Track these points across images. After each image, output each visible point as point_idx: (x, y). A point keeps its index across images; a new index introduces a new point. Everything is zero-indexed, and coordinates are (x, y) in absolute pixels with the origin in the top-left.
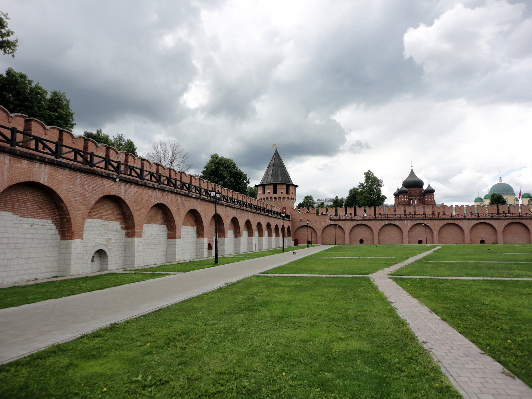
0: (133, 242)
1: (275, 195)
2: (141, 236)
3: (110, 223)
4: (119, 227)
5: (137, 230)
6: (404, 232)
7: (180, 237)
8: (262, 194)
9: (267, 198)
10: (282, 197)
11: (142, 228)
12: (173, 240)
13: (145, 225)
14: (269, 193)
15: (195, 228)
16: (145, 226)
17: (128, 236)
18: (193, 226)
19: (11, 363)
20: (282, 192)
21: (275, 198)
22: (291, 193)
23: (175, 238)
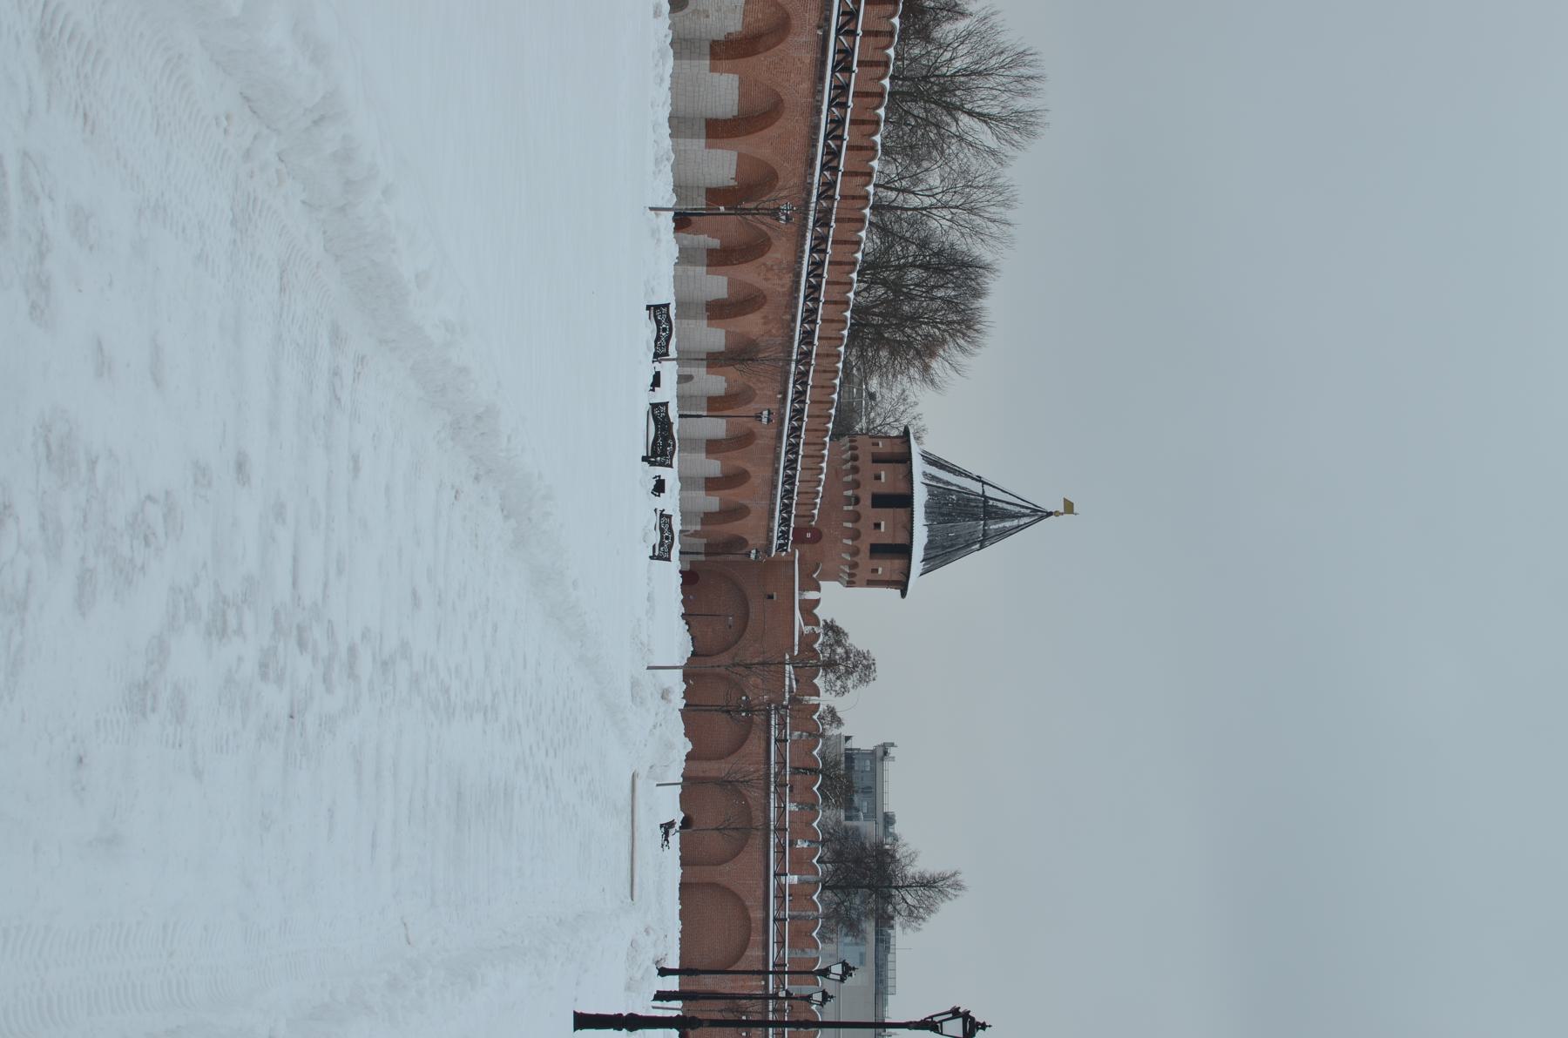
0: (700, 56)
1: (866, 501)
2: (713, 69)
3: (739, 16)
4: (732, 30)
5: (725, 63)
6: (733, 759)
7: (708, 146)
8: (875, 449)
9: (855, 470)
10: (858, 525)
11: (729, 71)
12: (704, 131)
13: (736, 77)
14: (878, 477)
15: (733, 183)
16: (725, 279)
17: (714, 45)
18: (735, 179)
19: (725, 221)
20: (877, 526)
21: (857, 501)
22: (875, 563)
23: (708, 136)
